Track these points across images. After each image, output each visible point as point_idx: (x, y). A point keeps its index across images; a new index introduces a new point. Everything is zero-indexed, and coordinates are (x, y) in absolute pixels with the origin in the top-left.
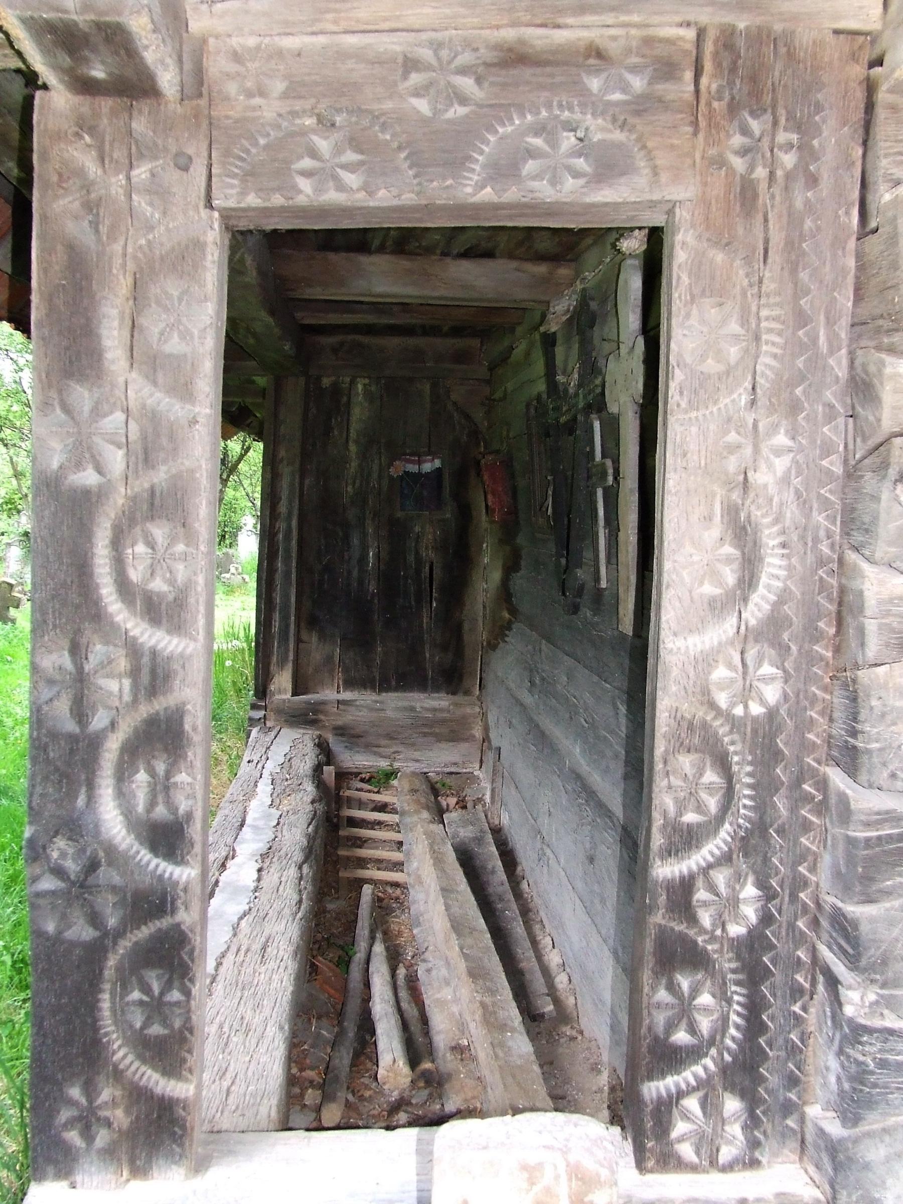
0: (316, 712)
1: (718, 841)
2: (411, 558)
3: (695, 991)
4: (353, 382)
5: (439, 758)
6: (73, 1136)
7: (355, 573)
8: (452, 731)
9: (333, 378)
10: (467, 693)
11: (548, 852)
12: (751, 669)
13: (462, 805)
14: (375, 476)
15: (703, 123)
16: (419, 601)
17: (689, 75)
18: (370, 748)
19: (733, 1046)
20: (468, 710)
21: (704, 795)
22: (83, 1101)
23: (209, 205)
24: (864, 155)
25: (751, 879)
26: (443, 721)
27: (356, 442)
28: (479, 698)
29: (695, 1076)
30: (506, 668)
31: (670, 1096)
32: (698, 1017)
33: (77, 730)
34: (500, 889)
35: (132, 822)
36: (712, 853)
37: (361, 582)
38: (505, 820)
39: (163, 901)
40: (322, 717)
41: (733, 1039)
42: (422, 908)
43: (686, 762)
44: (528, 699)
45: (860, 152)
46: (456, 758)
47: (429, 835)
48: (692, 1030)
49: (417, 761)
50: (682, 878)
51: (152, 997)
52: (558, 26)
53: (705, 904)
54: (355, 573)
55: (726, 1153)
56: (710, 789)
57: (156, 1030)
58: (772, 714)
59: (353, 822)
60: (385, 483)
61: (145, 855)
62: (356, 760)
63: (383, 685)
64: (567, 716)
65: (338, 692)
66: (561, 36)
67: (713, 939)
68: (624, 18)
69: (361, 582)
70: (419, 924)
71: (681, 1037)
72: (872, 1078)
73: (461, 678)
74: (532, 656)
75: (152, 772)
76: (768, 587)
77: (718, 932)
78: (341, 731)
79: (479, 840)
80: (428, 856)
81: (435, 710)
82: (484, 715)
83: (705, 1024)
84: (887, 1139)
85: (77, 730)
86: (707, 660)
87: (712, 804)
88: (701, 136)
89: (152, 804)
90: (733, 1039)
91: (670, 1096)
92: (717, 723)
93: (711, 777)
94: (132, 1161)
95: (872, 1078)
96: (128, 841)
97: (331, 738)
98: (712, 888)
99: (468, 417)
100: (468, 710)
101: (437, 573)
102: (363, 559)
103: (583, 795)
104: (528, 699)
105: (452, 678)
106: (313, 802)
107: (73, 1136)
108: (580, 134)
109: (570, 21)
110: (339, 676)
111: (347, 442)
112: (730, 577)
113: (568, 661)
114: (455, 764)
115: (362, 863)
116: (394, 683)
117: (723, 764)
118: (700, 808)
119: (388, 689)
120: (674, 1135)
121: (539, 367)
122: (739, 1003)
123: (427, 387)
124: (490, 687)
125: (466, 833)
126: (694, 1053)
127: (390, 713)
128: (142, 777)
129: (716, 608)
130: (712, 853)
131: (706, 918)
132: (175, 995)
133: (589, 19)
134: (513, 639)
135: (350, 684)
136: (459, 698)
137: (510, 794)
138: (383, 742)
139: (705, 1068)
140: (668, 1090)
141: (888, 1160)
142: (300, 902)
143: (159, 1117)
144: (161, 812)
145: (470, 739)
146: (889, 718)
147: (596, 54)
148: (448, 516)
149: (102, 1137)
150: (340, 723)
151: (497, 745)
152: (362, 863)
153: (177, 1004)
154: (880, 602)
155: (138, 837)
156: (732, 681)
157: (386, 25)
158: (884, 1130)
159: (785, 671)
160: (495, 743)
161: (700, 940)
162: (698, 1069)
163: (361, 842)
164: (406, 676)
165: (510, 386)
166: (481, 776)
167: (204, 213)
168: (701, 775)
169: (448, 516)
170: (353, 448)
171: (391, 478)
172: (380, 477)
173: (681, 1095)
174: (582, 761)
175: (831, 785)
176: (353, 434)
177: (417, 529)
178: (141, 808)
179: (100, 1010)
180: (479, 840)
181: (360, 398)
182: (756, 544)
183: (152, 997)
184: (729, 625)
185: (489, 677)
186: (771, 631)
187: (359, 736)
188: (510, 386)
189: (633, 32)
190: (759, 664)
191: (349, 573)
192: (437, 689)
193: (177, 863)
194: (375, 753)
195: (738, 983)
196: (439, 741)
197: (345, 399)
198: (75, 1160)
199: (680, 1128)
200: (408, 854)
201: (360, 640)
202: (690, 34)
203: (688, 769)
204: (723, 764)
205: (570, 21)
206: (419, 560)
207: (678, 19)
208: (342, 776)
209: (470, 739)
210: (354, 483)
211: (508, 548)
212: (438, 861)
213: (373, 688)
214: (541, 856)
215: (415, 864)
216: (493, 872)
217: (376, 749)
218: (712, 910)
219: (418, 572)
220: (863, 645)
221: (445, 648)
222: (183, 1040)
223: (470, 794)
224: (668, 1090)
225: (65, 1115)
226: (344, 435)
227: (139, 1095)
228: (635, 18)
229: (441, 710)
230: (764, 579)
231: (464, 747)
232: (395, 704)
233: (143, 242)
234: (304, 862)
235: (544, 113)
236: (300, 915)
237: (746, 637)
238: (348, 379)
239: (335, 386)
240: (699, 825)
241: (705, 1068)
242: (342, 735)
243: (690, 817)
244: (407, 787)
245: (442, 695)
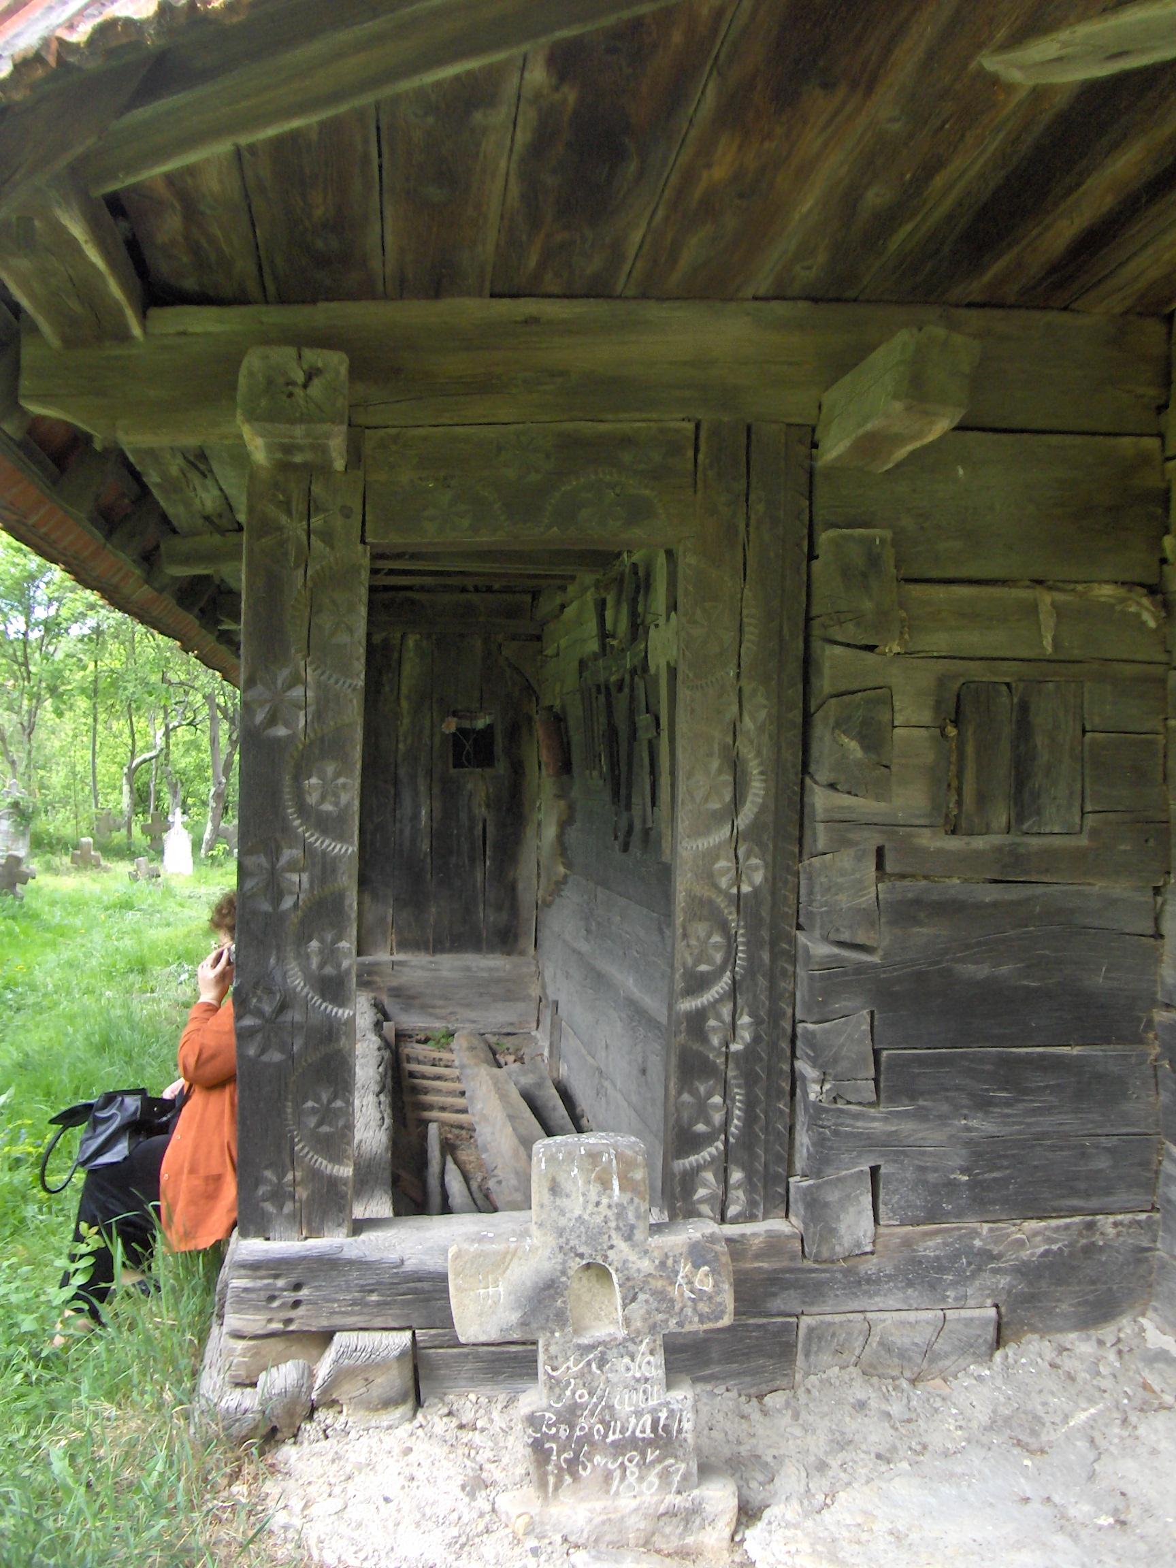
0: (369, 973)
1: (722, 984)
2: (463, 816)
3: (710, 1095)
4: (403, 636)
5: (498, 1016)
6: (269, 1207)
7: (407, 832)
8: (509, 991)
9: (384, 634)
10: (522, 953)
11: (607, 1084)
12: (741, 861)
13: (520, 1059)
14: (427, 732)
15: (700, 485)
16: (472, 860)
17: (690, 453)
18: (425, 1008)
19: (736, 1132)
20: (525, 970)
21: (711, 951)
22: (275, 1179)
23: (363, 541)
24: (811, 505)
25: (746, 1010)
26: (498, 981)
27: (408, 698)
28: (534, 958)
29: (710, 1154)
30: (563, 925)
31: (692, 1169)
32: (711, 1112)
33: (270, 909)
34: (562, 1122)
35: (308, 978)
36: (718, 993)
37: (413, 841)
38: (564, 1070)
39: (330, 1031)
40: (377, 979)
41: (736, 1127)
42: (489, 1139)
43: (701, 928)
44: (584, 947)
45: (807, 503)
46: (513, 1018)
47: (493, 1077)
48: (708, 1122)
49: (474, 1022)
50: (697, 1010)
51: (322, 1105)
52: (601, 421)
53: (714, 1029)
54: (407, 832)
55: (732, 1210)
56: (716, 947)
57: (325, 1129)
58: (756, 891)
59: (412, 1075)
60: (437, 740)
61: (317, 1000)
62: (413, 1021)
63: (438, 947)
64: (621, 953)
65: (392, 954)
66: (603, 427)
67: (719, 1054)
68: (644, 416)
69: (413, 841)
70: (486, 1150)
71: (701, 1127)
72: (829, 1144)
73: (516, 937)
74: (588, 904)
75: (322, 941)
76: (753, 802)
77: (724, 1049)
78: (396, 992)
79: (540, 1085)
80: (493, 1093)
81: (490, 969)
82: (539, 974)
83: (718, 1118)
84: (840, 1185)
85: (270, 909)
86: (712, 855)
87: (718, 957)
88: (699, 494)
89: (322, 966)
90: (736, 1127)
91: (692, 1169)
92: (719, 900)
93: (717, 938)
94: (309, 1224)
95: (829, 1144)
96: (306, 990)
97: (386, 1000)
98: (719, 1017)
99: (517, 670)
100: (525, 970)
101: (491, 830)
102: (415, 817)
103: (637, 1017)
104: (584, 947)
105: (506, 939)
106: (379, 1049)
107: (269, 1207)
108: (618, 490)
109: (610, 417)
110: (393, 938)
111: (398, 699)
112: (728, 797)
113: (623, 901)
114: (512, 1024)
115: (430, 1107)
116: (448, 945)
117: (724, 927)
118: (710, 961)
119: (443, 950)
120: (696, 1197)
121: (592, 626)
122: (740, 1101)
123: (478, 643)
124: (547, 942)
125: (527, 1080)
126: (709, 1139)
127: (445, 973)
128: (314, 944)
129: (717, 818)
130: (718, 993)
131: (715, 1041)
132: (339, 1103)
133: (622, 416)
134: (567, 892)
135: (403, 945)
136: (515, 959)
137: (570, 1044)
138: (441, 1003)
139: (717, 1148)
140: (691, 1164)
141: (840, 1200)
142: (383, 1118)
143: (328, 1191)
144: (329, 970)
145: (526, 998)
146: (833, 890)
147: (627, 441)
148: (502, 772)
149: (288, 1207)
150: (395, 984)
151: (555, 998)
152: (430, 1107)
153: (340, 1109)
154: (826, 810)
155: (312, 986)
156: (729, 869)
157: (485, 421)
158: (838, 1179)
159: (765, 861)
160: (552, 997)
161: (711, 1056)
162: (712, 1150)
163: (426, 1091)
164: (460, 937)
165: (563, 643)
166: (539, 1036)
167: (360, 547)
168: (709, 938)
169: (502, 772)
170: (404, 704)
171: (443, 734)
172: (432, 735)
173: (699, 1168)
174: (635, 990)
175: (799, 941)
176: (404, 690)
177: (470, 786)
178: (314, 966)
179: (285, 1113)
180: (540, 1085)
181: (411, 654)
182: (745, 773)
183: (322, 1105)
184: (726, 832)
185: (545, 934)
186: (754, 833)
187: (413, 998)
188: (563, 643)
189: (652, 424)
190: (748, 857)
191: (401, 831)
192: (492, 949)
193: (340, 1006)
194: (431, 1015)
195: (739, 1086)
196: (494, 1001)
197: (396, 655)
198: (269, 1221)
199: (702, 1192)
200: (471, 1099)
201: (413, 899)
202: (690, 426)
203: (702, 935)
204: (724, 927)
205: (610, 417)
206: (472, 819)
207: (681, 416)
208: (401, 1036)
209: (526, 998)
210: (405, 740)
211: (562, 803)
212: (503, 1097)
213: (427, 949)
214: (599, 1092)
215: (479, 1106)
216: (554, 1108)
217: (430, 1010)
218: (720, 1035)
219: (471, 829)
220: (815, 841)
221: (499, 908)
222: (344, 1136)
223: (527, 1051)
224: (691, 1164)
225: (262, 1190)
226: (395, 692)
227: (315, 1175)
228: (654, 416)
229: (497, 969)
230: (750, 798)
231: (521, 1006)
232: (450, 965)
233: (318, 567)
234: (380, 1093)
235: (593, 477)
236: (385, 1127)
237: (736, 839)
238: (398, 635)
239: (385, 640)
240: (708, 972)
241: (717, 1148)
242: (397, 996)
243: (703, 968)
244: (465, 1044)
245: (497, 955)
